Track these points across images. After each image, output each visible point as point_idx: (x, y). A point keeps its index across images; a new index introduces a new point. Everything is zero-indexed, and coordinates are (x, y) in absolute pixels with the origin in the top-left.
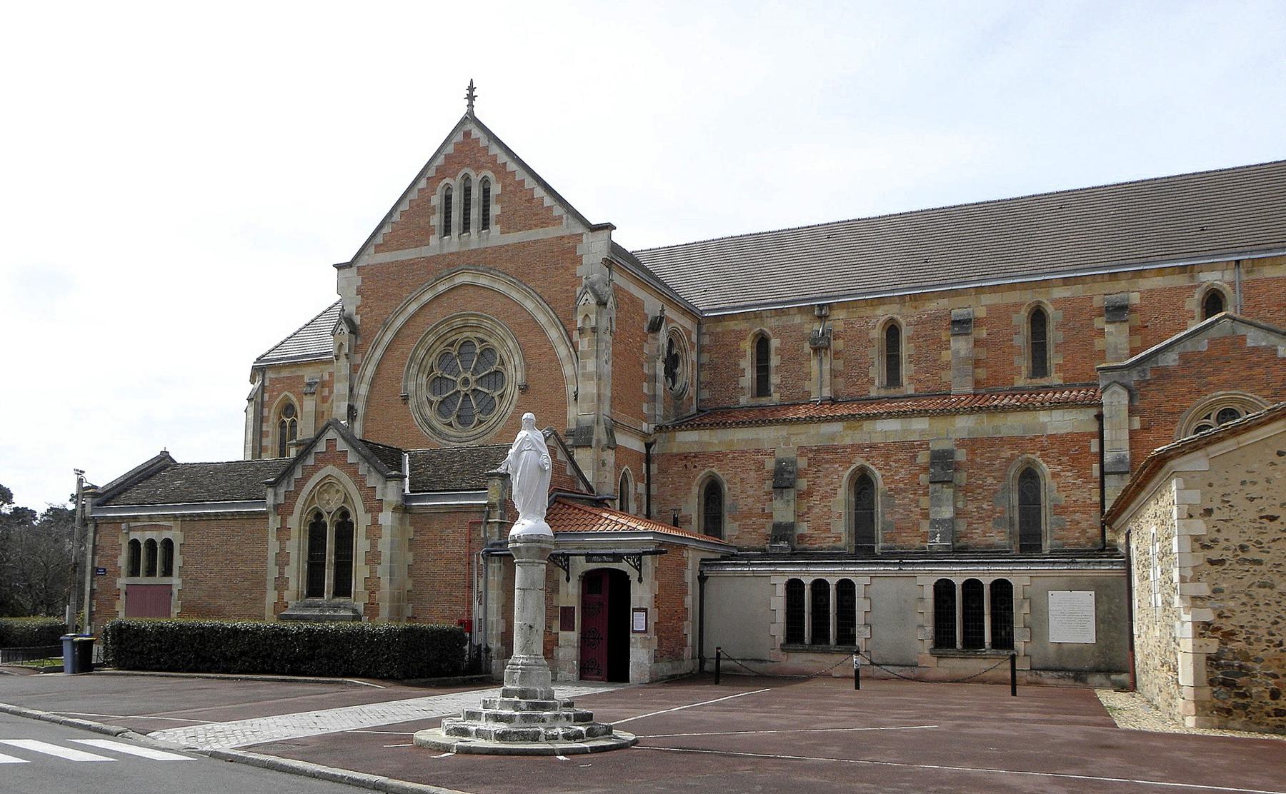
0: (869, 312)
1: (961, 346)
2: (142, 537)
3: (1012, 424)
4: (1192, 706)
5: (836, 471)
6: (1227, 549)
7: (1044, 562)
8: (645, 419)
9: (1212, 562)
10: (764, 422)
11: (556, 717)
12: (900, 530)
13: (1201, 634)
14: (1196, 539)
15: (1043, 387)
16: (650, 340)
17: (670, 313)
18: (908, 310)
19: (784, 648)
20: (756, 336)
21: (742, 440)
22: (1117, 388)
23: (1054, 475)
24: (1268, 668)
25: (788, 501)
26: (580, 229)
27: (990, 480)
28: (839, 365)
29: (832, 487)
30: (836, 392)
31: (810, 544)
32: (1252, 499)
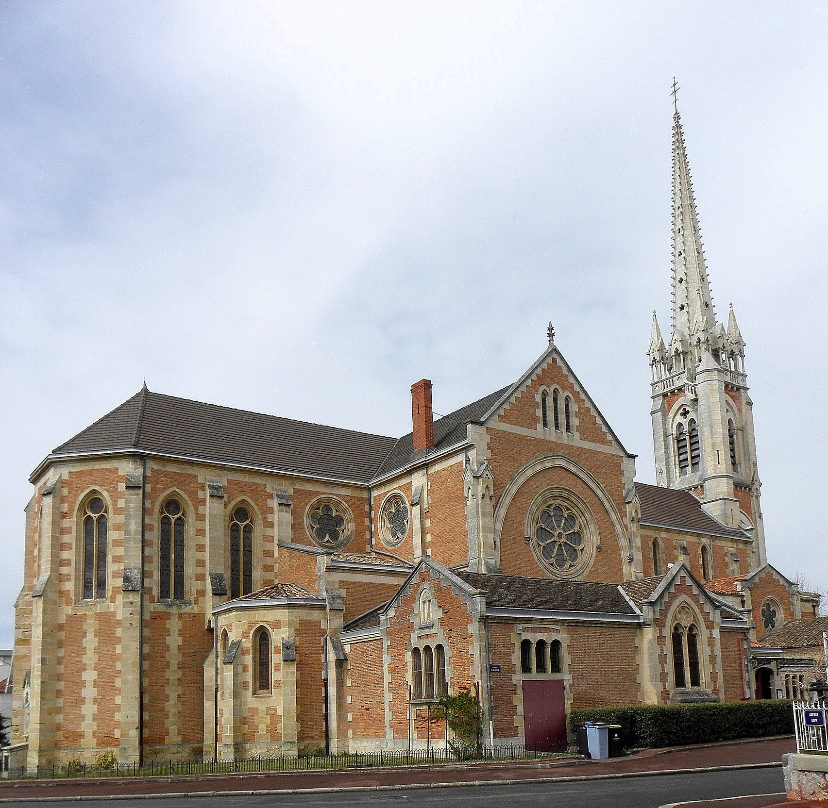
2: (534, 638)
26: (622, 454)
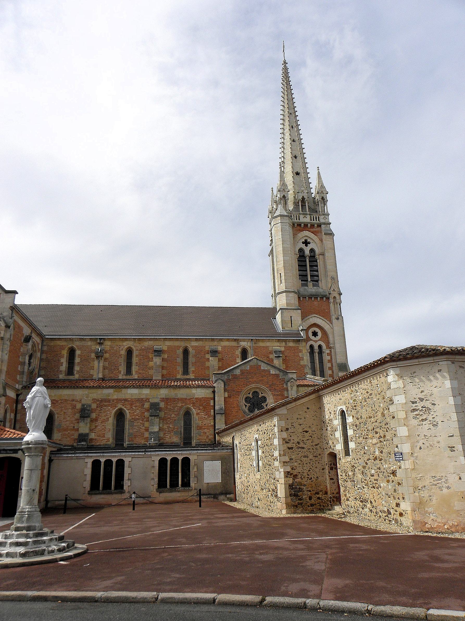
0: (120, 343)
1: (157, 360)
3: (182, 393)
4: (284, 505)
5: (109, 410)
6: (293, 443)
7: (202, 449)
8: (18, 382)
9: (289, 448)
10: (77, 387)
11: (51, 540)
12: (135, 436)
13: (287, 476)
14: (284, 439)
15: (187, 379)
16: (24, 346)
17: (34, 335)
18: (137, 344)
19: (89, 493)
20: (69, 348)
21: (66, 395)
22: (220, 381)
23: (198, 414)
24: (308, 488)
25: (86, 423)
27: (173, 415)
28: (107, 364)
29: (107, 417)
30: (104, 375)
31: (95, 443)
32: (300, 425)
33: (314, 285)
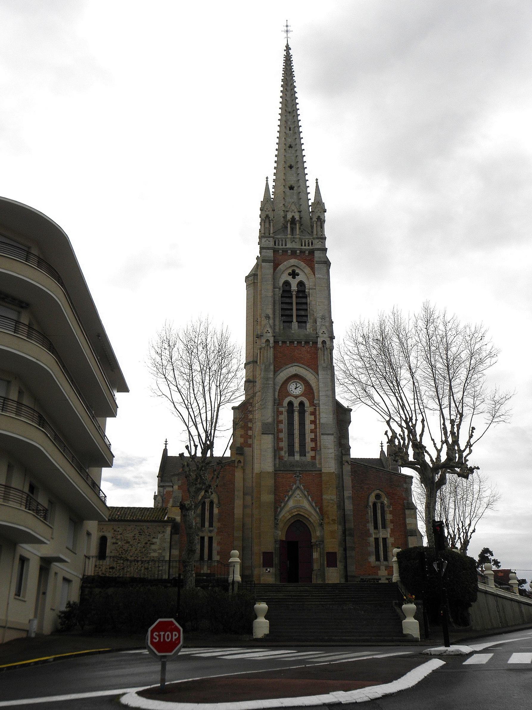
33: (299, 327)
